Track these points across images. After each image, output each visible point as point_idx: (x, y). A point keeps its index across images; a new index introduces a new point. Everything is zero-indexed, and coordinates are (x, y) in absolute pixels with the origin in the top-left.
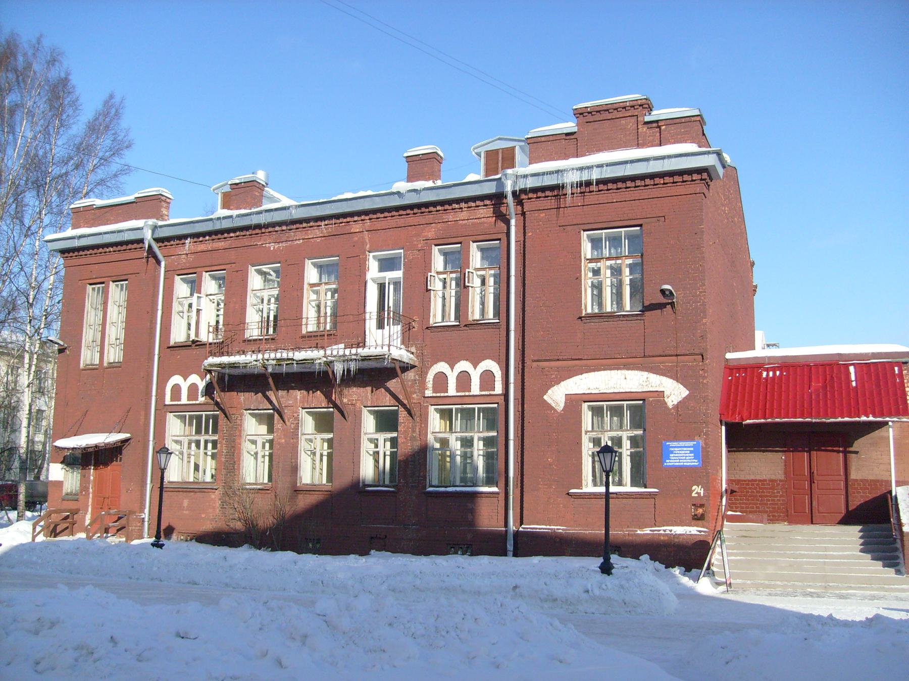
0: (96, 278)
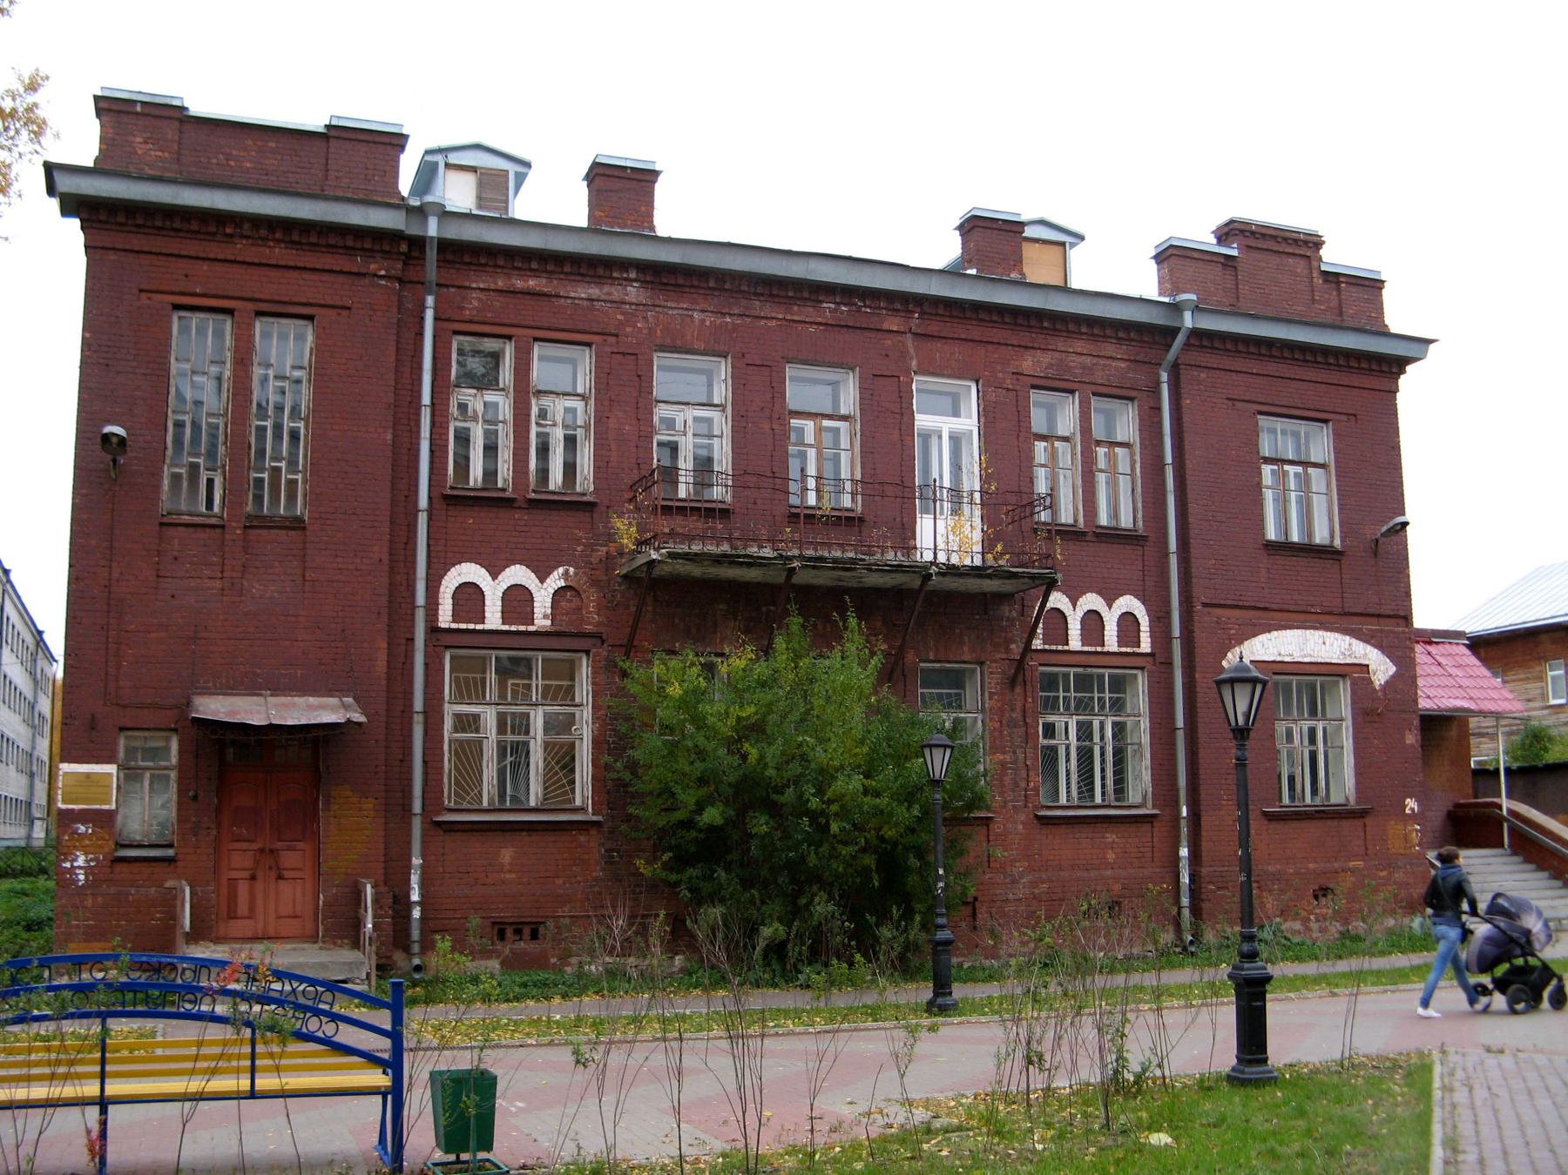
0: (471, 322)
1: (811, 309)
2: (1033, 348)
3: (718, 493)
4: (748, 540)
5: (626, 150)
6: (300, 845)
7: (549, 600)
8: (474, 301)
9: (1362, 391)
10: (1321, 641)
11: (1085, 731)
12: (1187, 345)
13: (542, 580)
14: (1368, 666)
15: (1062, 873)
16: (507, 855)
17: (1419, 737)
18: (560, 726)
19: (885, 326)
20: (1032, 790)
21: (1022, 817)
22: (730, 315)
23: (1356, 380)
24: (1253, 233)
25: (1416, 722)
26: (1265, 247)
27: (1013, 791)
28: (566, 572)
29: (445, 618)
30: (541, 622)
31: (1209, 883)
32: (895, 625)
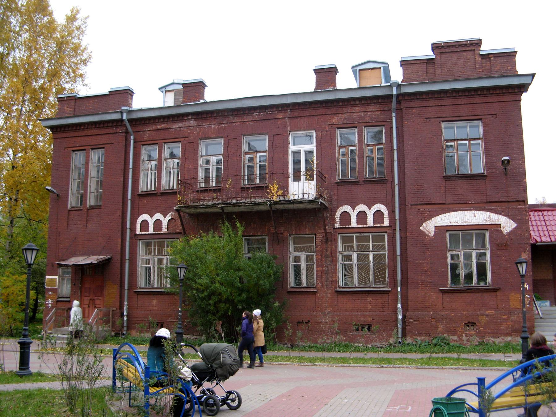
0: (146, 141)
1: (250, 116)
2: (337, 114)
3: (213, 183)
4: (228, 198)
5: (325, 62)
6: (100, 298)
7: (167, 223)
8: (147, 134)
9: (499, 103)
10: (473, 215)
11: (160, 261)
12: (399, 102)
13: (165, 217)
14: (500, 224)
15: (346, 313)
16: (155, 302)
17: (530, 255)
18: (481, 255)
19: (277, 117)
20: (334, 281)
21: (330, 291)
22: (224, 124)
23: (495, 99)
24: (443, 47)
25: (529, 248)
26: (450, 51)
27: (326, 281)
28: (172, 214)
29: (138, 231)
30: (164, 230)
31: (410, 318)
32: (279, 223)
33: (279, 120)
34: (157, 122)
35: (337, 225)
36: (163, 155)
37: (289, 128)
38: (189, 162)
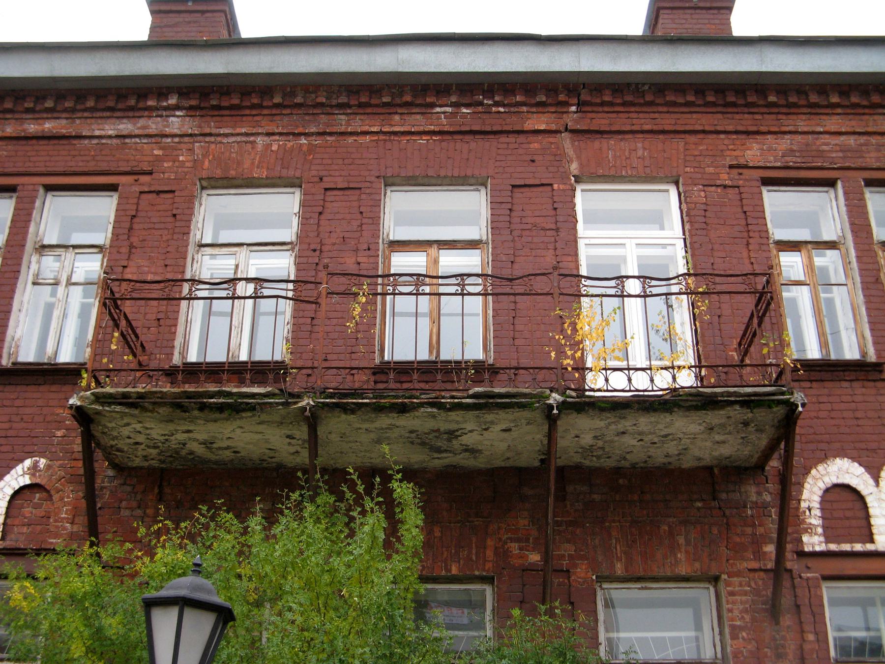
2: (758, 133)
19: (529, 125)
28: (35, 467)
33: (531, 138)
34: (28, 111)
35: (814, 542)
36: (32, 229)
37: (574, 167)
38: (141, 262)
